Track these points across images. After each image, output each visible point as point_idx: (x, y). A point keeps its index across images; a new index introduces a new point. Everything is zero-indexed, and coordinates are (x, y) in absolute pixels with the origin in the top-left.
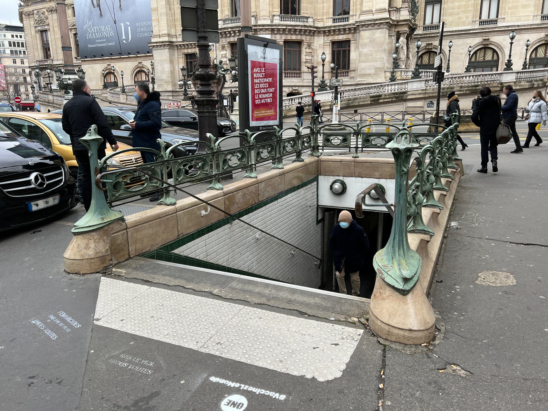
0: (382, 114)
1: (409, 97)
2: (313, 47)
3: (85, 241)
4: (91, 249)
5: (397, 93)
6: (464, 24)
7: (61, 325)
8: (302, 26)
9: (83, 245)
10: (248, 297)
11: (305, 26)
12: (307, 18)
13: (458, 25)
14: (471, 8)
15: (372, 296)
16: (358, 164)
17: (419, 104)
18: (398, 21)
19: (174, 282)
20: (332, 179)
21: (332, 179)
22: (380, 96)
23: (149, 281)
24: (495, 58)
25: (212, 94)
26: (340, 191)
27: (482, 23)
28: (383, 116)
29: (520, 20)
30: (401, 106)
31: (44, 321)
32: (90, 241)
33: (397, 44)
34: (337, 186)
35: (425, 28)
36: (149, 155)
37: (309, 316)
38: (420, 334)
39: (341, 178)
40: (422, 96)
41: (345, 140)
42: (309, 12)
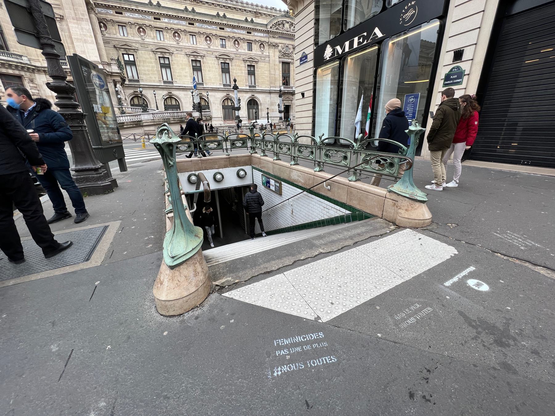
0: (134, 135)
1: (144, 124)
2: (36, 83)
3: (191, 269)
4: (200, 274)
5: (135, 122)
6: (154, 81)
7: (299, 349)
8: (17, 62)
9: (192, 274)
10: (347, 243)
11: (21, 63)
12: (21, 56)
13: (151, 81)
14: (156, 72)
15: (52, 259)
16: (230, 159)
17: (152, 128)
18: (111, 73)
19: (288, 261)
20: (187, 174)
21: (187, 174)
22: (124, 123)
23: (269, 272)
24: (177, 104)
25: (77, 108)
26: (240, 176)
27: (165, 82)
28: (134, 136)
29: (185, 84)
30: (140, 130)
31: (282, 361)
32: (196, 265)
33: (116, 89)
34: (193, 178)
35: (130, 81)
36: (61, 173)
37: (381, 235)
38: (429, 221)
39: (193, 172)
40: (152, 123)
41: (219, 145)
42: (19, 51)
